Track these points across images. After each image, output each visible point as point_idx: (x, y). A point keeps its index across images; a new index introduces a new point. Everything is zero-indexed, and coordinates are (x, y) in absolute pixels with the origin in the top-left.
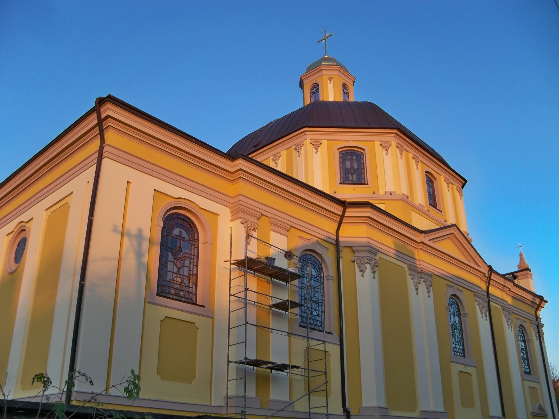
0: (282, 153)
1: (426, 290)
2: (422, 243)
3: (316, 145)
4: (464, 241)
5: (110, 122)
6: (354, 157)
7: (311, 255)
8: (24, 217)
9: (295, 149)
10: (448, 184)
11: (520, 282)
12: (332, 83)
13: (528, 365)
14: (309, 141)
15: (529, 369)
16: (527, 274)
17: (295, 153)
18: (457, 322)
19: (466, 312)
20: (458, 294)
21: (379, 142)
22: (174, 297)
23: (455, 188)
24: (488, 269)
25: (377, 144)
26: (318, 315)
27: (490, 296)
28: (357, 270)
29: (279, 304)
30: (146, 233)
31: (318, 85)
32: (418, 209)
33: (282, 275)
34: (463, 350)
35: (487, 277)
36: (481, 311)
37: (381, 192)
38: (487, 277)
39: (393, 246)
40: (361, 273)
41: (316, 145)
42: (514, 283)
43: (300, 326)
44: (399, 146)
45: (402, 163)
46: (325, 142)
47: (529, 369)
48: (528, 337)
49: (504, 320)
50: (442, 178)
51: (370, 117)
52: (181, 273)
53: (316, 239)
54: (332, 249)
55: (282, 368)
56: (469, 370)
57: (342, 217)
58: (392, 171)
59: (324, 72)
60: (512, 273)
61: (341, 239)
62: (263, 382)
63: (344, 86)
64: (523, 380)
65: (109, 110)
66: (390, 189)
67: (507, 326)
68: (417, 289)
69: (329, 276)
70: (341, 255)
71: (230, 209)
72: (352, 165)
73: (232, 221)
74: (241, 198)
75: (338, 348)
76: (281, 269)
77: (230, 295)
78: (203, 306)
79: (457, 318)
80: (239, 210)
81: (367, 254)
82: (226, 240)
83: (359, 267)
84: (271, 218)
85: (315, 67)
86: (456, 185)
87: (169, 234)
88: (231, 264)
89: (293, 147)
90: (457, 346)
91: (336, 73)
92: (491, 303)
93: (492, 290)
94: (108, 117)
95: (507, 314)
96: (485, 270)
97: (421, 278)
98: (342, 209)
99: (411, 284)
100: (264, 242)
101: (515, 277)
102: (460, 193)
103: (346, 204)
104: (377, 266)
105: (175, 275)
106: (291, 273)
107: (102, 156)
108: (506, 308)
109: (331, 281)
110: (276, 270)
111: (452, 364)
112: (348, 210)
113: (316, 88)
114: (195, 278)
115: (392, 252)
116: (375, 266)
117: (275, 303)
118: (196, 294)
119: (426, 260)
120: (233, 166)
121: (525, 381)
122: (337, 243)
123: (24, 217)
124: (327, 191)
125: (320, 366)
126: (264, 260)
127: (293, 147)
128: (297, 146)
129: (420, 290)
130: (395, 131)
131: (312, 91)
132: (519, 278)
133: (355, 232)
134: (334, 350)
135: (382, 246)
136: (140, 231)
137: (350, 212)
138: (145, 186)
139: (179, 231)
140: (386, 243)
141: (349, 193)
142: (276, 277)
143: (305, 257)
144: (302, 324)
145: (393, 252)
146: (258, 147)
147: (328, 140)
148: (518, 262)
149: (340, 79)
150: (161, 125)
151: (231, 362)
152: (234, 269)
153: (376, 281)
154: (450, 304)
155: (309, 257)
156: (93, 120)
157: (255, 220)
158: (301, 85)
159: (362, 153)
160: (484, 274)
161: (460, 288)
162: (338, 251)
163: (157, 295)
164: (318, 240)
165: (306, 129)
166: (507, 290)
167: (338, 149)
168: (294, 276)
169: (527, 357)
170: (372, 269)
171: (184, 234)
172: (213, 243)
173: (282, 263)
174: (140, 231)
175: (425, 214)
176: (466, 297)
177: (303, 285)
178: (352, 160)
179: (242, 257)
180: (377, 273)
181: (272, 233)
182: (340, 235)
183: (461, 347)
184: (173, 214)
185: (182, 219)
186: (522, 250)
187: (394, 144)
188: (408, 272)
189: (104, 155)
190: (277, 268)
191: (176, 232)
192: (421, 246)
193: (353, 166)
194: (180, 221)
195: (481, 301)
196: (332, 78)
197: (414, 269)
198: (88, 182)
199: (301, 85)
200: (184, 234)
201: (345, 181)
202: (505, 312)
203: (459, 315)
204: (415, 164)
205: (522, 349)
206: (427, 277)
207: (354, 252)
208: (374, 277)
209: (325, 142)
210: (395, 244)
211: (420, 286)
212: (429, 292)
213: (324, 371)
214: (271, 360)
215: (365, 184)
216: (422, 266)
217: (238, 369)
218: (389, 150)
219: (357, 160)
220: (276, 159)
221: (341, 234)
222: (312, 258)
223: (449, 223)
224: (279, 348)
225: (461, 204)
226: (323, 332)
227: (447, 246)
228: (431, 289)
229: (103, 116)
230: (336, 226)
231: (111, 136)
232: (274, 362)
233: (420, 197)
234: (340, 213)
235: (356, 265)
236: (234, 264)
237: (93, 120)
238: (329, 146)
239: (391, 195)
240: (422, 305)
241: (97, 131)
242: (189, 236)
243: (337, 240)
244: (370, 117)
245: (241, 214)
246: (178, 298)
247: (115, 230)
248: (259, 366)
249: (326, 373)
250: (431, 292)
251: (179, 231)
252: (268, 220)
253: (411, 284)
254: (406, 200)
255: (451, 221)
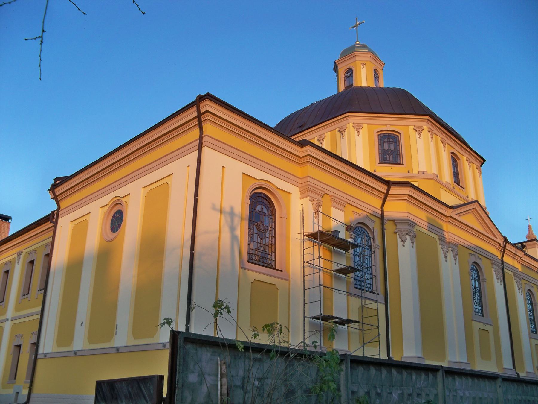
0: (326, 134)
1: (453, 258)
2: (451, 217)
3: (358, 129)
4: (482, 213)
5: (208, 116)
6: (391, 140)
7: (362, 227)
8: (120, 192)
9: (339, 131)
10: (469, 163)
11: (529, 251)
12: (365, 68)
13: (535, 325)
14: (351, 125)
15: (535, 328)
16: (535, 244)
17: (338, 134)
18: (477, 286)
19: (485, 278)
20: (479, 262)
21: (413, 127)
22: (262, 264)
23: (475, 166)
24: (503, 240)
25: (411, 128)
26: (367, 279)
27: (504, 264)
28: (399, 240)
29: (342, 269)
30: (238, 210)
31: (352, 70)
32: (445, 186)
33: (344, 246)
34: (482, 310)
35: (502, 247)
36: (497, 276)
37: (415, 172)
38: (502, 247)
39: (425, 220)
40: (402, 243)
41: (358, 129)
42: (524, 252)
43: (355, 288)
44: (430, 130)
45: (432, 145)
46: (365, 126)
47: (535, 328)
48: (535, 300)
49: (516, 285)
50: (465, 158)
51: (402, 103)
52: (264, 243)
53: (366, 213)
54: (378, 221)
55: (344, 322)
56: (487, 327)
57: (387, 194)
58: (424, 153)
59: (357, 58)
60: (521, 243)
61: (385, 214)
62: (331, 334)
63: (375, 71)
64: (530, 338)
65: (207, 106)
66: (422, 169)
67: (518, 291)
68: (446, 257)
69: (376, 245)
70: (385, 228)
71: (300, 188)
72: (389, 147)
73: (301, 198)
74: (309, 179)
75: (384, 306)
76: (344, 240)
77: (304, 262)
78: (282, 271)
79: (477, 282)
80: (307, 190)
81: (408, 227)
82: (298, 216)
83: (400, 238)
84: (332, 196)
85: (349, 52)
86: (476, 164)
87: (253, 210)
88: (304, 236)
89: (337, 130)
90: (477, 307)
91: (369, 59)
92: (505, 270)
93: (507, 259)
94: (207, 111)
95: (518, 279)
96: (501, 241)
97: (450, 247)
98: (386, 187)
99: (441, 252)
100: (327, 216)
101: (524, 247)
102: (480, 171)
103: (391, 183)
104: (415, 237)
105: (259, 245)
106: (351, 243)
107: (202, 144)
108: (517, 274)
109: (377, 249)
110: (340, 241)
111: (474, 322)
112: (392, 188)
113: (350, 72)
114: (273, 247)
115: (425, 225)
116: (414, 237)
117: (338, 268)
118: (275, 261)
119: (452, 232)
120: (302, 152)
121: (532, 340)
122: (382, 218)
123: (120, 192)
124: (368, 169)
125: (373, 321)
126: (331, 233)
127: (337, 130)
128: (341, 128)
129: (448, 257)
130: (427, 117)
131: (346, 75)
132: (528, 247)
133: (397, 208)
134: (382, 308)
135: (415, 218)
136: (232, 208)
137: (394, 190)
138: (236, 169)
139: (262, 206)
140: (420, 216)
141: (388, 172)
142: (338, 247)
143: (357, 229)
144: (356, 286)
145: (426, 224)
146: (303, 128)
147: (368, 124)
148: (526, 233)
149: (372, 65)
150: (248, 118)
151: (307, 317)
152: (306, 239)
153: (414, 250)
154: (472, 269)
155: (358, 228)
156: (193, 113)
157: (320, 198)
158: (336, 69)
159: (398, 136)
160: (500, 244)
161: (480, 256)
162: (383, 224)
163: (248, 262)
164: (368, 214)
165: (349, 114)
166: (518, 258)
167: (377, 132)
168: (354, 246)
169: (534, 318)
170: (411, 239)
171: (265, 211)
172: (287, 218)
173: (343, 235)
174: (232, 208)
175: (451, 191)
176: (484, 264)
177: (356, 253)
178: (389, 143)
179: (316, 230)
180: (415, 243)
181: (333, 209)
182: (385, 210)
183: (480, 308)
184: (256, 193)
185: (263, 198)
186: (530, 222)
187: (426, 129)
188: (438, 242)
189: (204, 144)
190: (341, 239)
191: (259, 208)
192: (450, 220)
193: (390, 148)
194: (261, 200)
195: (497, 268)
196: (365, 64)
197: (442, 239)
198: (189, 166)
199: (336, 69)
200: (265, 211)
201: (383, 161)
202: (516, 278)
203: (479, 280)
204: (443, 147)
205: (530, 311)
206: (454, 248)
207: (396, 225)
208: (413, 247)
209: (365, 126)
210: (428, 218)
211: (448, 254)
212: (455, 260)
213: (377, 325)
214: (334, 315)
215: (400, 164)
216: (450, 237)
217: (310, 324)
218: (422, 134)
219: (393, 142)
220: (321, 138)
221: (385, 209)
222: (363, 230)
223: (470, 200)
224: (342, 305)
225: (480, 181)
226: (375, 293)
227: (470, 220)
228: (457, 256)
229: (202, 111)
230: (380, 202)
231: (208, 128)
232: (341, 317)
233: (447, 177)
234: (385, 191)
235: (398, 236)
236: (306, 236)
237: (193, 113)
238: (369, 131)
239: (423, 174)
240: (450, 272)
241: (196, 122)
242: (268, 212)
243: (382, 214)
244: (402, 103)
245: (310, 194)
246: (262, 264)
247: (214, 208)
248: (327, 321)
249: (378, 328)
250: (457, 259)
251: (262, 206)
252: (330, 198)
253: (441, 252)
254: (436, 179)
255: (472, 197)
